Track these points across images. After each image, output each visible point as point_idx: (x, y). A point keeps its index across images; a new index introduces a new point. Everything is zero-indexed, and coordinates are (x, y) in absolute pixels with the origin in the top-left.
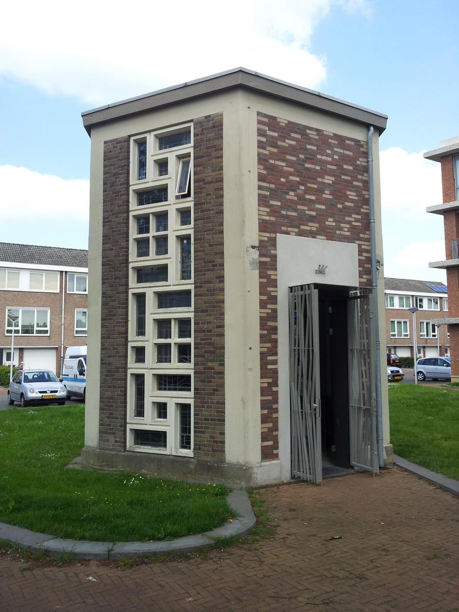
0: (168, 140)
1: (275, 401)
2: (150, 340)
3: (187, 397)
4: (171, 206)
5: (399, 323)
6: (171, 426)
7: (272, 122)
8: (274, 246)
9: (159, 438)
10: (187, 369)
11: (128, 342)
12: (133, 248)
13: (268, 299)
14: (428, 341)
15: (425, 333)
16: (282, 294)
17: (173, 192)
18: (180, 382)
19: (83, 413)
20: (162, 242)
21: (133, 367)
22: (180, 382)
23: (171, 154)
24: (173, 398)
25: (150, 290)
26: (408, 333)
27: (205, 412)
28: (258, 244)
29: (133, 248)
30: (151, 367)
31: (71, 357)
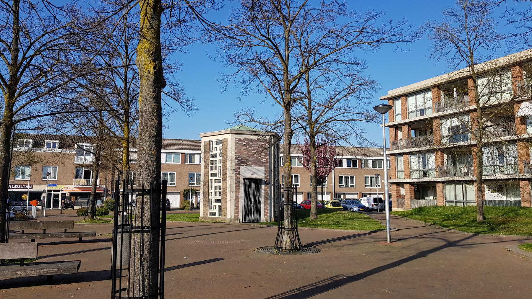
0: (218, 142)
1: (239, 205)
2: (213, 191)
3: (220, 204)
4: (218, 158)
5: (347, 178)
6: (216, 211)
7: (240, 140)
8: (239, 169)
9: (213, 214)
10: (220, 198)
11: (163, 270)
12: (210, 168)
13: (237, 181)
14: (372, 190)
15: (370, 184)
16: (241, 180)
17: (218, 155)
18: (219, 200)
19: (199, 212)
20: (216, 166)
21: (210, 198)
22: (219, 200)
23: (218, 146)
24: (218, 204)
25: (214, 178)
26: (354, 184)
27: (223, 207)
28: (107, 281)
29: (210, 168)
30: (213, 197)
31: (110, 248)
